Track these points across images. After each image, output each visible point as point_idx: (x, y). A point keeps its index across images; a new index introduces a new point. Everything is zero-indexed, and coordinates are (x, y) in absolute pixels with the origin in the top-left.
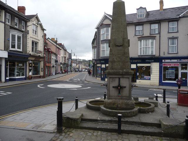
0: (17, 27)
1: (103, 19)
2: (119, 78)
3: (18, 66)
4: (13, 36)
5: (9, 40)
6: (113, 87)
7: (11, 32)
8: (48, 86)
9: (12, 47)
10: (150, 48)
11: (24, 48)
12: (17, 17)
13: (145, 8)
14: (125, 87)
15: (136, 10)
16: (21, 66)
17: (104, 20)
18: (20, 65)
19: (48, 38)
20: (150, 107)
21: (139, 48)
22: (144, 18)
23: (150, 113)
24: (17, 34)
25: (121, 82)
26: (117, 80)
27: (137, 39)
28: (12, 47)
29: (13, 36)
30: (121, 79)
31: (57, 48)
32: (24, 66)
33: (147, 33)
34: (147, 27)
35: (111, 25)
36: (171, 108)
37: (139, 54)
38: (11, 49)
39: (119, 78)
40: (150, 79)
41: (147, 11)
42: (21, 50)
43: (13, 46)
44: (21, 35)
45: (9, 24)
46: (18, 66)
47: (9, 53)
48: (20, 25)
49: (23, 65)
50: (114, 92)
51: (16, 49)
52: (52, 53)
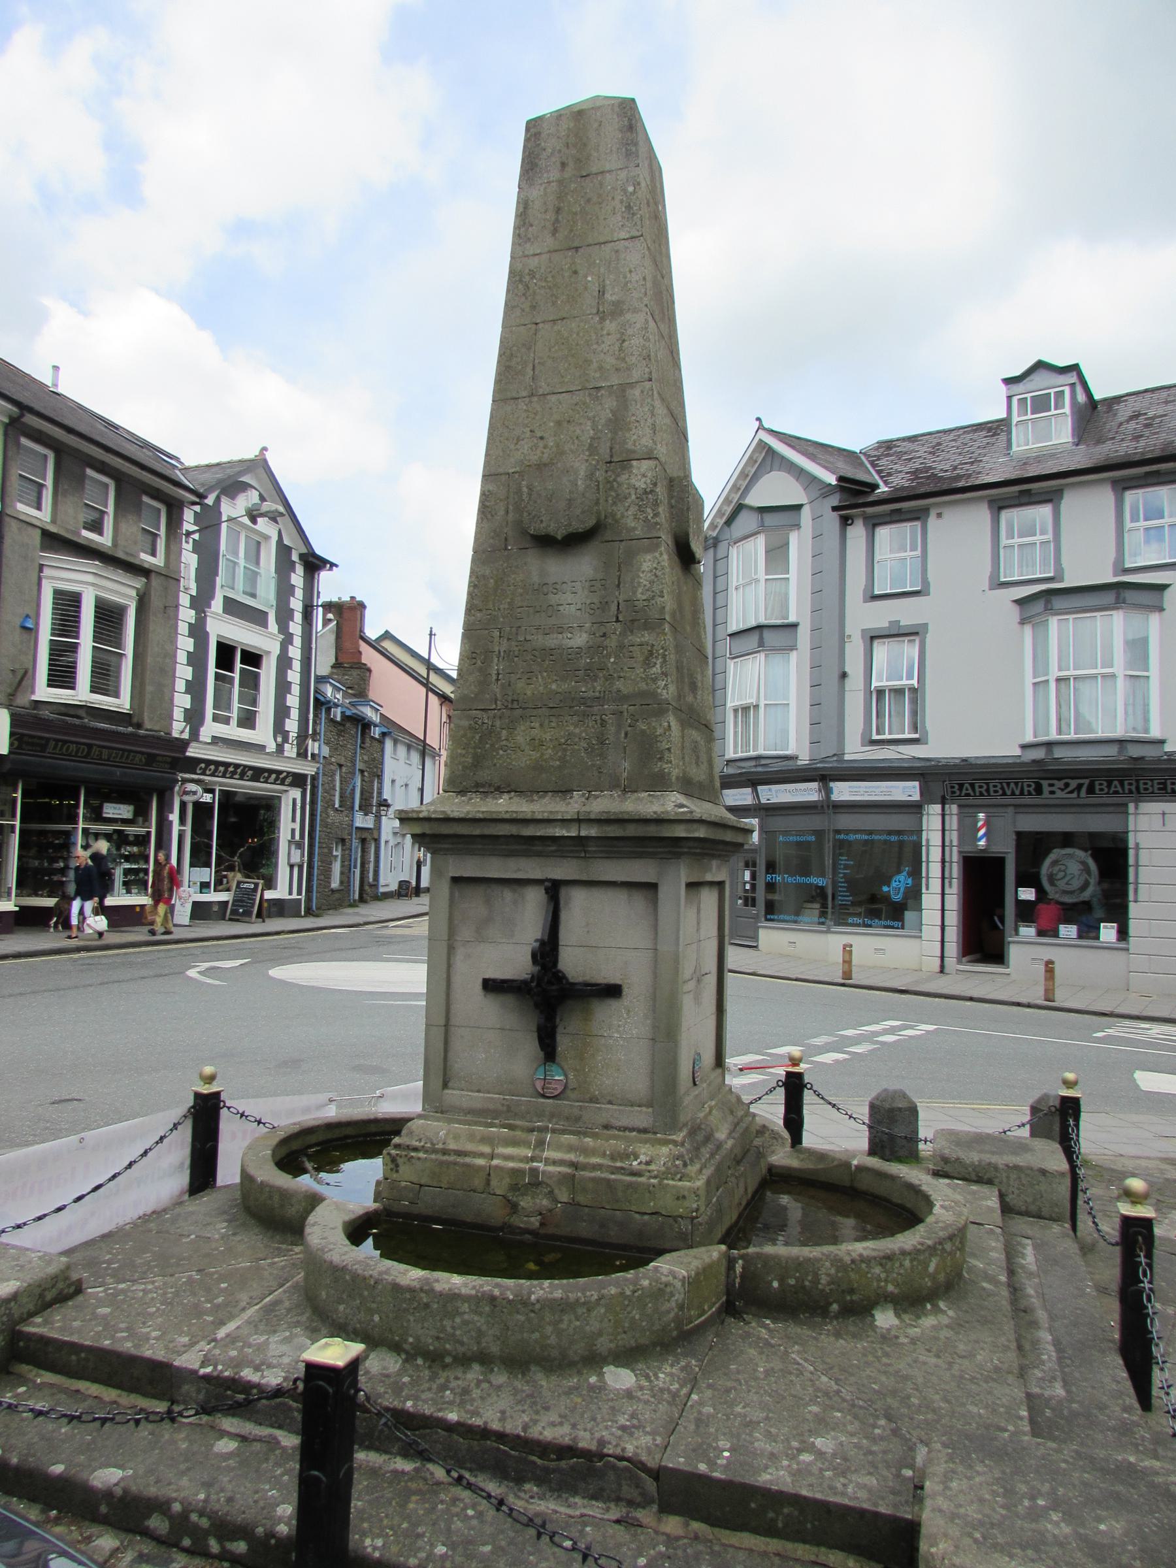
0: (104, 540)
1: (743, 474)
2: (554, 890)
3: (96, 815)
4: (68, 604)
5: (30, 632)
6: (491, 986)
7: (47, 572)
8: (272, 973)
9: (52, 683)
10: (1120, 683)
11: (149, 688)
12: (103, 468)
13: (1075, 368)
14: (613, 991)
15: (1003, 390)
16: (125, 821)
17: (755, 478)
18: (112, 810)
19: (387, 636)
20: (907, 1240)
21: (1029, 680)
22: (1051, 437)
23: (885, 1319)
24: (90, 584)
25: (569, 935)
26: (534, 902)
27: (1014, 612)
28: (52, 683)
29: (68, 604)
30: (577, 904)
31: (434, 700)
32: (147, 819)
33: (1088, 565)
34: (1088, 514)
35: (806, 513)
36: (525, 1427)
37: (1029, 738)
38: (43, 692)
39: (554, 890)
40: (903, 928)
41: (1097, 397)
42: (123, 702)
43: (62, 675)
44: (124, 591)
45: (44, 516)
46: (96, 815)
47: (17, 721)
48: (123, 526)
49: (141, 812)
50: (497, 1046)
51: (82, 693)
52: (392, 730)
